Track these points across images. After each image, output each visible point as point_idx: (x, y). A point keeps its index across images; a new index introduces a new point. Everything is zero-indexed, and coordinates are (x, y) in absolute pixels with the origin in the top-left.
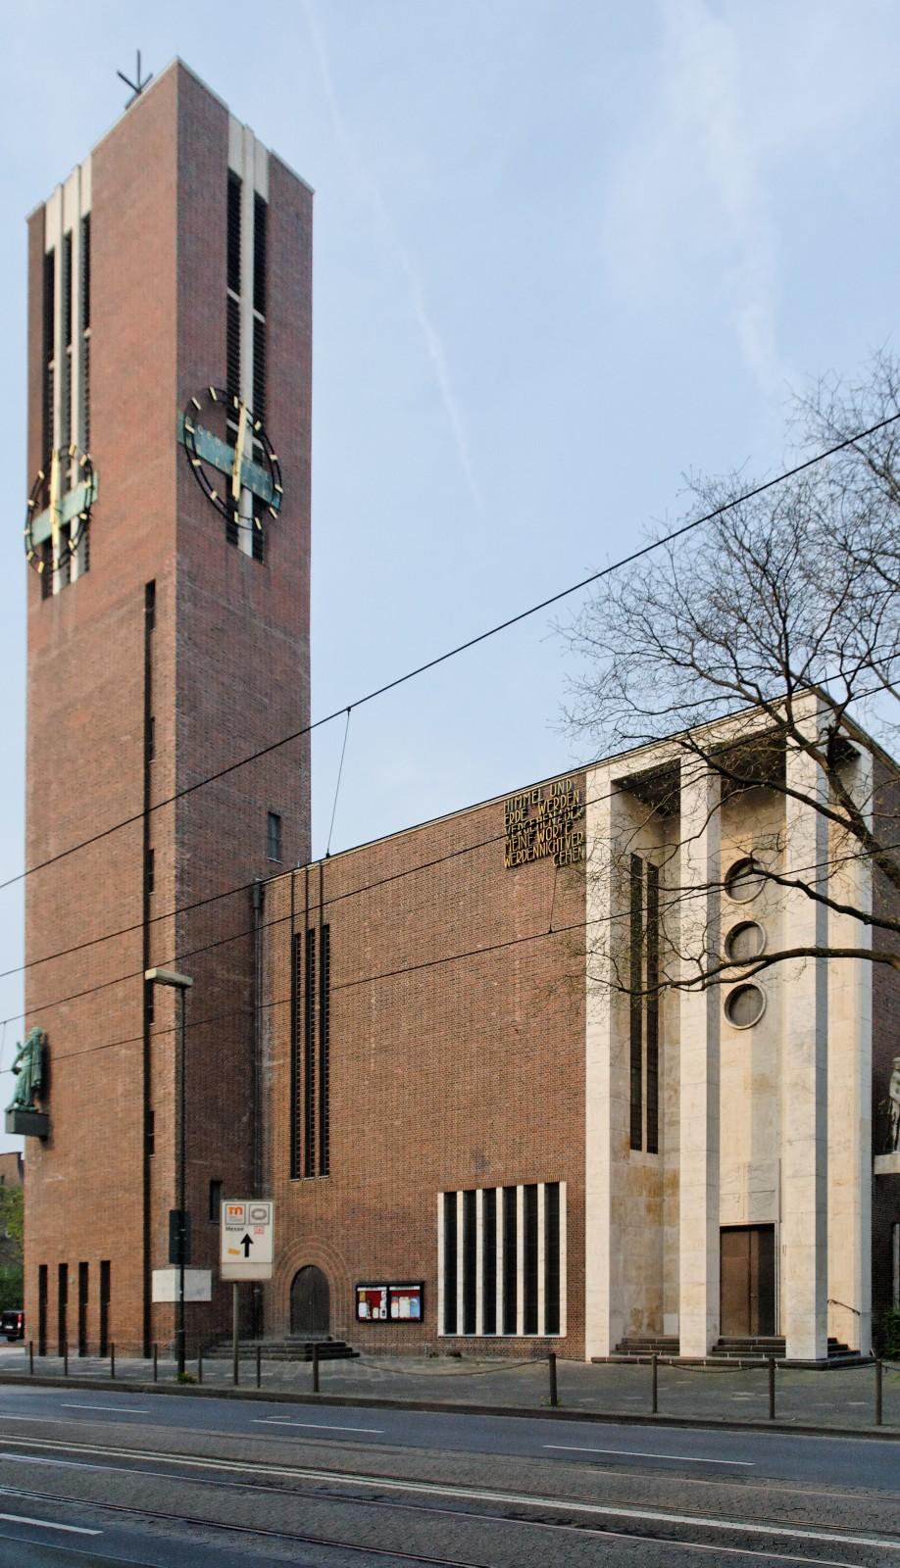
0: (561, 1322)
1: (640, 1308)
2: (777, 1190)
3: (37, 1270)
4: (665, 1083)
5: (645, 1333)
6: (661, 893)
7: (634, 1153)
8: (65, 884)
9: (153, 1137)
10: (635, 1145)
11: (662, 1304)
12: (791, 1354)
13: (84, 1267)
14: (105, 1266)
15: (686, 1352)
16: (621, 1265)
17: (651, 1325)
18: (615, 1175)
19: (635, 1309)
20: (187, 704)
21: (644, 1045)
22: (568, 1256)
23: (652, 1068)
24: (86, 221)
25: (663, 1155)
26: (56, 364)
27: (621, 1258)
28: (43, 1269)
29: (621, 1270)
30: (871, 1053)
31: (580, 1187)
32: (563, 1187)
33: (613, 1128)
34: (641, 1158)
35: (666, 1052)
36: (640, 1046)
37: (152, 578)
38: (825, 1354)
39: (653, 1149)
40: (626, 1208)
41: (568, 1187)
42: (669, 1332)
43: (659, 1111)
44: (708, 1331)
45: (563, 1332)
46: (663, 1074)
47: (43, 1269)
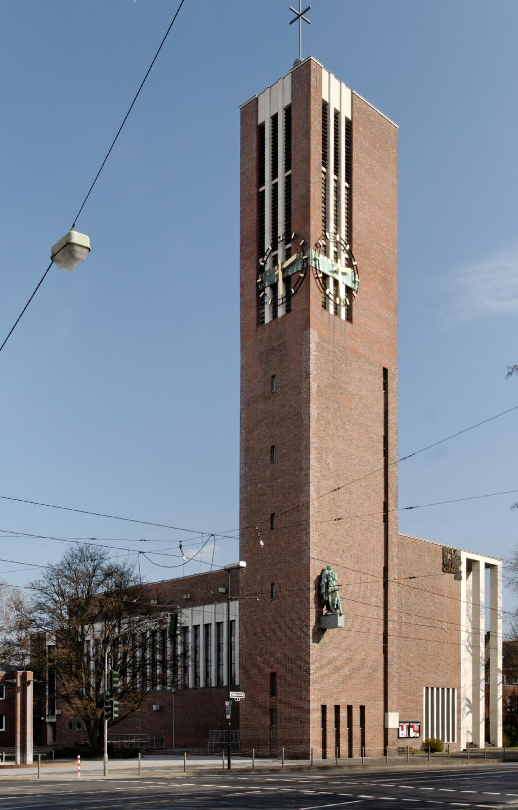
3: (320, 708)
8: (321, 529)
9: (384, 512)
13: (350, 708)
14: (362, 708)
20: (401, 750)
24: (288, 110)
26: (267, 188)
28: (324, 707)
37: (382, 368)
47: (324, 707)
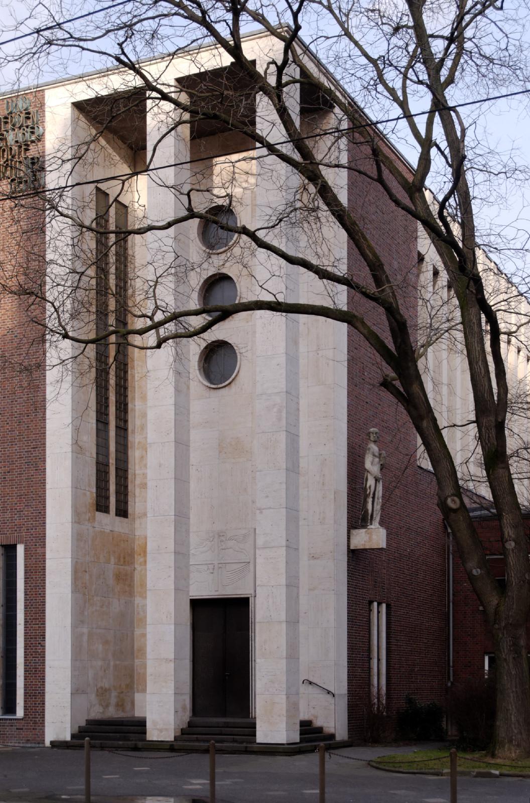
0: (18, 701)
1: (107, 686)
2: (252, 562)
4: (137, 441)
5: (112, 713)
6: (130, 318)
7: (99, 515)
10: (102, 506)
11: (132, 682)
12: (262, 736)
15: (153, 734)
16: (85, 638)
17: (120, 705)
18: (78, 538)
19: (102, 688)
21: (112, 398)
22: (26, 627)
23: (121, 473)
25: (134, 520)
27: (85, 630)
29: (85, 644)
30: (346, 421)
31: (39, 550)
32: (20, 549)
33: (76, 487)
34: (109, 521)
35: (137, 408)
36: (107, 399)
38: (296, 738)
39: (122, 512)
40: (91, 576)
41: (26, 550)
42: (138, 714)
43: (130, 471)
44: (176, 712)
45: (20, 712)
46: (133, 432)
